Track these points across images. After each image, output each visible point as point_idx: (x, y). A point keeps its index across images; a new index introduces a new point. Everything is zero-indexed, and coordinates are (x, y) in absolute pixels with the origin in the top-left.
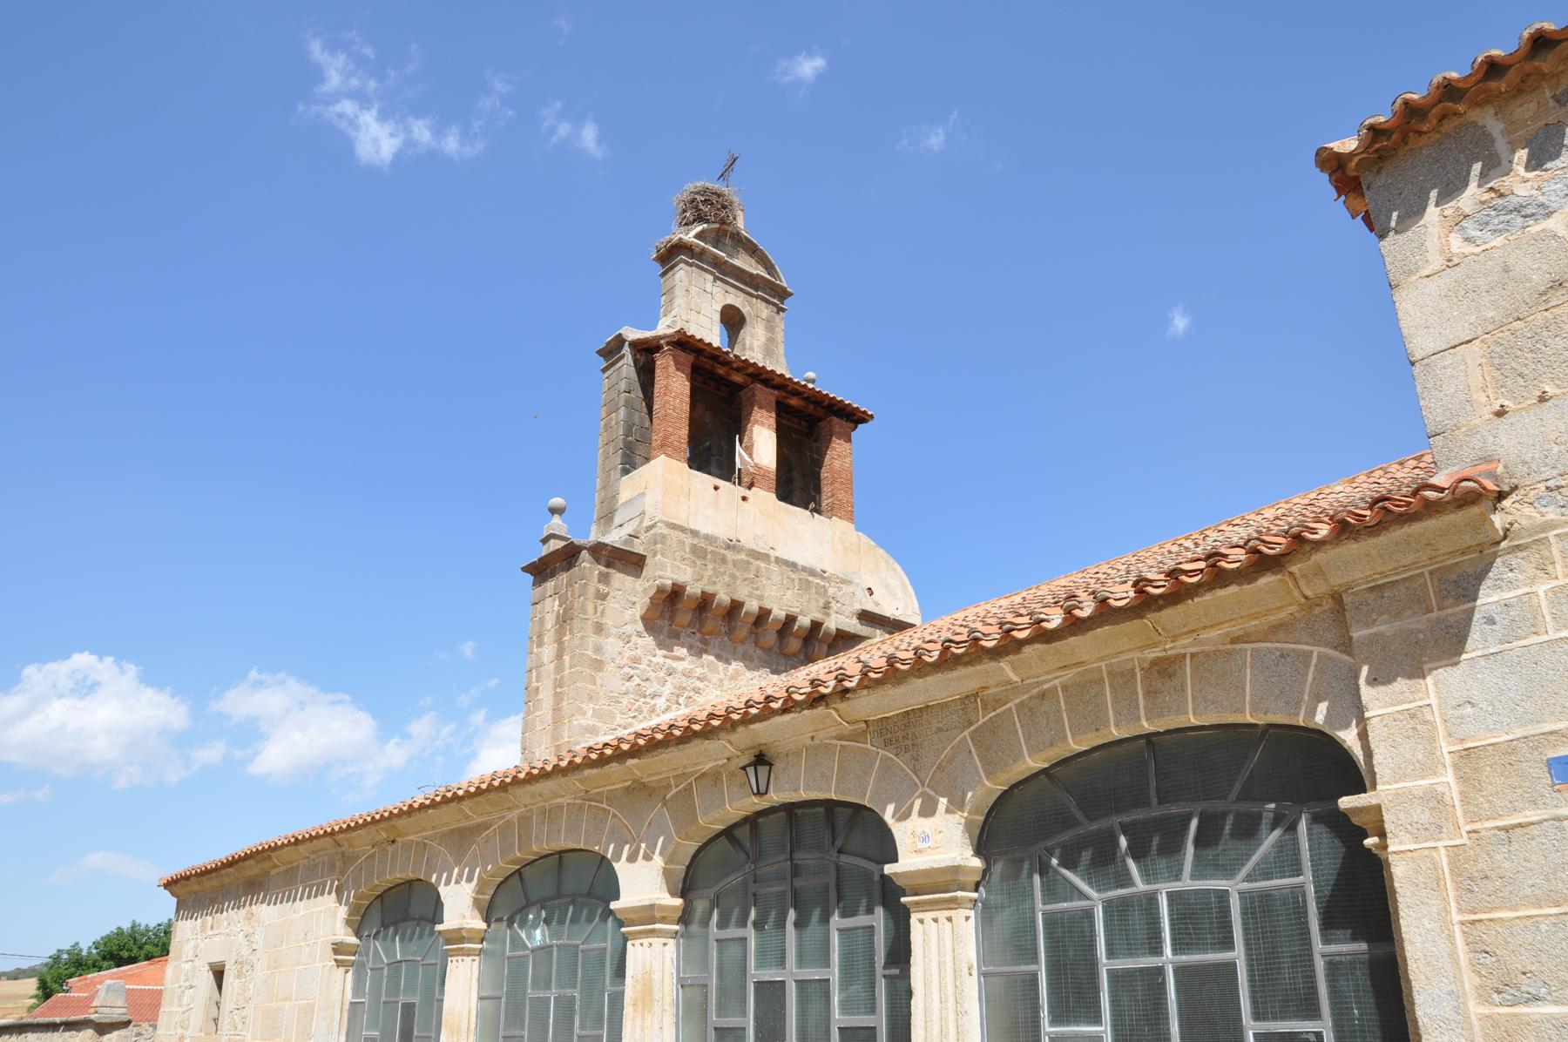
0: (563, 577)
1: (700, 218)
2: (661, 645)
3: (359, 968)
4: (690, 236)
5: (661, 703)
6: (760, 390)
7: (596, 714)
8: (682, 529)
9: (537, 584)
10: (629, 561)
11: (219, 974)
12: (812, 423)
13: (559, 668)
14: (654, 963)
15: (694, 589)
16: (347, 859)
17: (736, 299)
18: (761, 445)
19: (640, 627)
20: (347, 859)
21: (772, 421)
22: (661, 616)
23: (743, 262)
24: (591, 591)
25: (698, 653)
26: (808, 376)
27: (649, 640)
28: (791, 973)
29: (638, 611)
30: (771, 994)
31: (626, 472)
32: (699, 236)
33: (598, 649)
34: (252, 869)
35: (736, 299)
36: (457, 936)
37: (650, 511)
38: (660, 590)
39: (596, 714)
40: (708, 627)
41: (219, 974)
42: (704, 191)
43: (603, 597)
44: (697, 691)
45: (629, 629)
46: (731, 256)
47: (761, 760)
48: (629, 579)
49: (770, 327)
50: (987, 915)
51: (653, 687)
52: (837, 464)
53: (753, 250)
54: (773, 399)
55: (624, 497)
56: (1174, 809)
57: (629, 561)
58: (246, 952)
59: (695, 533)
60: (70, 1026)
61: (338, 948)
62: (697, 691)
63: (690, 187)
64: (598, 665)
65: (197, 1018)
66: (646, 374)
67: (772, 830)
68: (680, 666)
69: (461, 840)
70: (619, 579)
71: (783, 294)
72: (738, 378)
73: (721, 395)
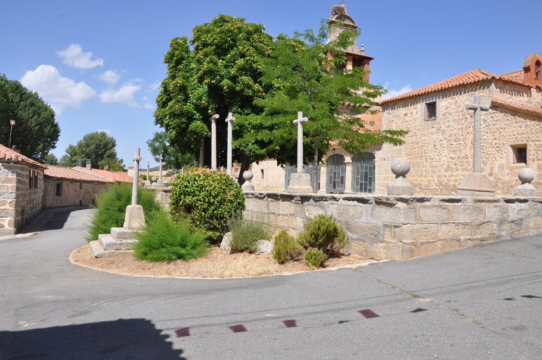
1: (336, 14)
4: (334, 19)
21: (352, 63)
23: (347, 22)
28: (336, 171)
30: (335, 173)
41: (262, 171)
42: (337, 8)
46: (344, 21)
50: (352, 166)
53: (349, 18)
56: (86, 173)
58: (267, 168)
63: (334, 6)
67: (335, 156)
71: (355, 27)
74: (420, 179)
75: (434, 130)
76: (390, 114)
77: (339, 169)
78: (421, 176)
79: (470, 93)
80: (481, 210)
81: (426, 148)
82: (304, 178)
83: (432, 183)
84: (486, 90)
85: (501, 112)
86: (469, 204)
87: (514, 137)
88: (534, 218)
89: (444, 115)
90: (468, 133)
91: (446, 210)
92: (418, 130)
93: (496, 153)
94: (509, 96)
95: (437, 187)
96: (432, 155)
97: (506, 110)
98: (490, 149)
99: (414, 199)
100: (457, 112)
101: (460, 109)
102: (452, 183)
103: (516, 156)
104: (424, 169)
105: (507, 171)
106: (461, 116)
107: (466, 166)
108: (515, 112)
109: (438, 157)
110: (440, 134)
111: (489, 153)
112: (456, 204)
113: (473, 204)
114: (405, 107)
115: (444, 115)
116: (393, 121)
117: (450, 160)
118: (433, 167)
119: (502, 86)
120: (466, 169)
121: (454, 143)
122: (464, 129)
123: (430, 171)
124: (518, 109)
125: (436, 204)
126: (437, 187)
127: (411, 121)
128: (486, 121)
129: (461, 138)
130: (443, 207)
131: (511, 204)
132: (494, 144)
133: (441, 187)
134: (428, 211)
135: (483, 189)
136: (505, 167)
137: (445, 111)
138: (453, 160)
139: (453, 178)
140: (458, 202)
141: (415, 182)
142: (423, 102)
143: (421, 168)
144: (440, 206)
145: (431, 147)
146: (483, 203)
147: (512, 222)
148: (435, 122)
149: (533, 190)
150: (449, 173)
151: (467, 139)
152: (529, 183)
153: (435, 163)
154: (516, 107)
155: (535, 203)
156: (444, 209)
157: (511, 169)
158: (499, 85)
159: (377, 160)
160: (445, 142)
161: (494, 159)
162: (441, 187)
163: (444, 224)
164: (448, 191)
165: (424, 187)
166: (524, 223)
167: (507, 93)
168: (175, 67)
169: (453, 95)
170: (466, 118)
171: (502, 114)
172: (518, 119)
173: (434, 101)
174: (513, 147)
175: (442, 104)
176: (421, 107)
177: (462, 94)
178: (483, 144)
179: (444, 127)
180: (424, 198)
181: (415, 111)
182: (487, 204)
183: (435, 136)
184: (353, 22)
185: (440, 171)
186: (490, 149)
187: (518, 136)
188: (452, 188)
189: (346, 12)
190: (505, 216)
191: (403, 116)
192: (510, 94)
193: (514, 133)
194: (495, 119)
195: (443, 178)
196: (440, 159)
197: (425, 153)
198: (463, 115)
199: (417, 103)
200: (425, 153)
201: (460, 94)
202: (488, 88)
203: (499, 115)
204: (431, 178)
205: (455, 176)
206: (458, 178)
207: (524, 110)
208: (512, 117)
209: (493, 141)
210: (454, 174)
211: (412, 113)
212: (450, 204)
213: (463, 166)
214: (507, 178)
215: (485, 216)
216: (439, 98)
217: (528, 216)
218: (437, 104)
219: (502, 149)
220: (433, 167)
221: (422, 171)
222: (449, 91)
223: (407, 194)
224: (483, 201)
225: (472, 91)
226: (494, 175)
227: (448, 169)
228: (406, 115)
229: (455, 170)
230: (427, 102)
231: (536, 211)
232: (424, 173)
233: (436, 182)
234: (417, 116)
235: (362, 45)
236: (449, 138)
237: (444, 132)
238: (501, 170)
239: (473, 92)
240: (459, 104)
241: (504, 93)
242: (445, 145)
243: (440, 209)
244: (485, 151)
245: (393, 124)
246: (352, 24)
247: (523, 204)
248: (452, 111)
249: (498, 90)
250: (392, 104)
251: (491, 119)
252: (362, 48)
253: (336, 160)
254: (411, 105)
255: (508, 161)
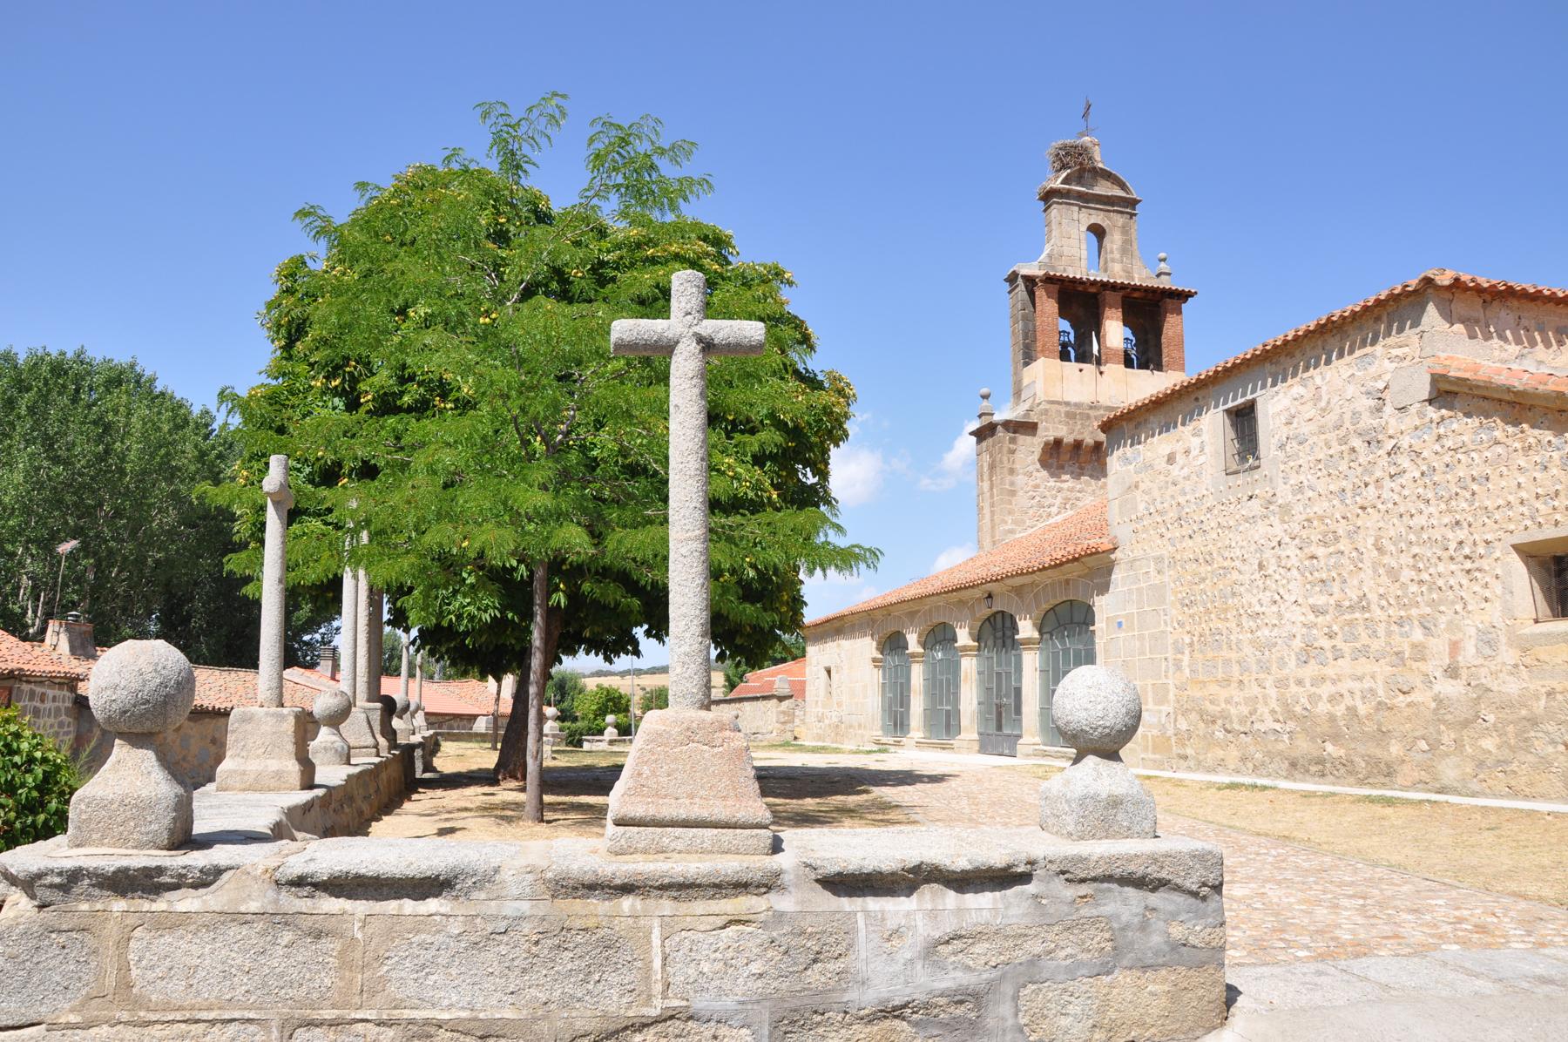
0: (990, 440)
1: (1064, 167)
2: (1052, 475)
3: (883, 668)
4: (1058, 184)
5: (1054, 510)
6: (1110, 296)
7: (1014, 522)
8: (1059, 403)
9: (979, 442)
10: (1028, 428)
11: (829, 672)
12: (1149, 310)
13: (992, 496)
14: (969, 666)
15: (1069, 439)
16: (874, 621)
17: (1097, 218)
18: (1115, 332)
19: (1038, 466)
20: (874, 621)
21: (1120, 314)
22: (1051, 456)
23: (1103, 189)
24: (1005, 450)
25: (1077, 476)
26: (1141, 276)
27: (1045, 473)
29: (1036, 456)
31: (1026, 364)
32: (1064, 182)
33: (1012, 484)
34: (837, 624)
35: (1097, 218)
36: (913, 655)
37: (1041, 396)
38: (1047, 444)
39: (1014, 522)
40: (1082, 459)
41: (829, 672)
42: (1064, 147)
43: (1013, 452)
44: (1078, 499)
45: (1031, 468)
47: (990, 596)
48: (1029, 439)
49: (1125, 230)
51: (1050, 501)
52: (1170, 333)
54: (1119, 299)
55: (1025, 382)
57: (1028, 428)
59: (1067, 404)
60: (765, 698)
61: (874, 660)
62: (1078, 499)
64: (1013, 493)
65: (822, 693)
66: (1031, 294)
67: (999, 617)
68: (1065, 485)
69: (912, 615)
70: (1021, 438)
71: (1133, 203)
72: (1093, 290)
73: (1081, 302)
74: (1223, 694)
75: (1256, 507)
76: (1127, 461)
77: (1008, 664)
78: (1226, 682)
79: (1358, 353)
80: (607, 945)
81: (1235, 575)
82: (264, 728)
83: (1263, 710)
84: (1410, 334)
85: (1468, 415)
86: (510, 908)
87: (1525, 509)
88: (1083, 985)
89: (1282, 447)
90: (1363, 508)
91: (331, 945)
92: (1209, 510)
93: (1465, 582)
94: (1513, 349)
95: (1278, 726)
96: (1254, 601)
97: (1485, 404)
98: (1441, 568)
99: (75, 876)
100: (1322, 431)
101: (1332, 418)
102: (1323, 708)
103: (1547, 593)
104: (1233, 655)
105: (1509, 655)
106: (1334, 444)
107: (1364, 638)
108: (1515, 406)
109: (1275, 608)
110: (1275, 520)
111: (1440, 583)
112: (408, 906)
113: (543, 908)
114: (1168, 430)
115: (1282, 447)
116: (1137, 487)
117: (1311, 617)
118: (1260, 647)
119: (1479, 313)
120: (1364, 652)
121: (1320, 551)
122: (1349, 494)
123: (1252, 661)
124: (1523, 394)
125: (254, 906)
126: (1278, 726)
127: (1187, 478)
128: (1418, 454)
129: (1342, 529)
130: (306, 923)
131: (873, 904)
132: (1453, 545)
133: (1291, 725)
134: (185, 948)
135: (668, 811)
136: (1503, 639)
137: (1285, 431)
138: (1321, 618)
139: (1326, 690)
140: (423, 897)
141: (1211, 708)
142: (1216, 406)
143: (1225, 653)
144: (279, 920)
145: (1249, 571)
146: (627, 903)
147: (894, 1012)
148: (1257, 475)
149: (1115, 803)
150: (1312, 670)
151: (1362, 532)
152: (1112, 755)
153: (1266, 632)
154: (1518, 385)
155: (1084, 889)
156: (318, 935)
157: (1525, 646)
158: (1459, 307)
159: (1100, 626)
160: (1291, 551)
161: (1459, 607)
162: (1291, 725)
163: (311, 1024)
164: (1313, 739)
165: (1237, 727)
166: (1000, 1012)
167: (1502, 337)
168: (289, 346)
169: (1307, 369)
170: (1353, 450)
171: (1474, 422)
172: (1533, 434)
173: (1249, 397)
174: (1530, 554)
175: (1276, 405)
176: (1212, 424)
177: (1335, 363)
178: (1415, 550)
179: (1284, 494)
180: (160, 870)
181: (1195, 442)
182: (666, 906)
183: (1261, 528)
184: (1123, 186)
185: (1282, 663)
186: (1441, 568)
187: (1538, 505)
188: (1325, 728)
189: (1097, 157)
190: (815, 976)
191: (1161, 464)
192: (1518, 342)
193: (1524, 495)
194: (1449, 443)
195: (1294, 688)
196: (1280, 616)
197: (1234, 594)
198: (1343, 441)
199: (1200, 414)
200: (1234, 594)
201: (1328, 362)
202: (1416, 324)
203: (1463, 427)
204: (1256, 690)
205: (1334, 682)
206: (1343, 687)
207: (1546, 397)
208: (1510, 429)
209: (1450, 535)
210: (1329, 671)
211: (1187, 452)
212: (360, 907)
213: (1356, 639)
214: (1512, 687)
215: (647, 978)
216: (1264, 387)
217: (1032, 971)
218: (1259, 407)
219: (1484, 564)
220: (1260, 647)
221: (1227, 662)
222: (1291, 355)
223: (123, 841)
224: (627, 889)
225: (1363, 344)
226: (1464, 673)
227: (1308, 653)
228: (1171, 459)
229: (1330, 655)
230: (1230, 405)
231: (1098, 939)
232: (1236, 669)
233: (1274, 704)
234: (1202, 459)
235: (1162, 255)
236: (1304, 534)
237: (1286, 509)
238: (1487, 651)
239: (1368, 349)
240: (1325, 398)
241: (1488, 337)
242: (1294, 561)
243: (287, 937)
244: (1425, 576)
245: (1138, 493)
246: (1122, 194)
247: (982, 903)
248: (1306, 429)
249: (1459, 327)
250: (1132, 425)
251: (1437, 447)
252: (1163, 265)
253: (999, 634)
254: (1183, 424)
255: (1508, 612)
